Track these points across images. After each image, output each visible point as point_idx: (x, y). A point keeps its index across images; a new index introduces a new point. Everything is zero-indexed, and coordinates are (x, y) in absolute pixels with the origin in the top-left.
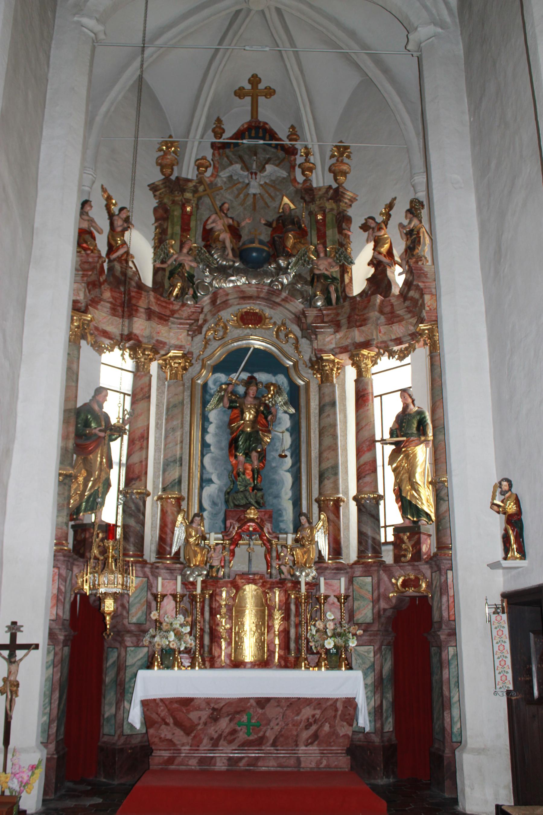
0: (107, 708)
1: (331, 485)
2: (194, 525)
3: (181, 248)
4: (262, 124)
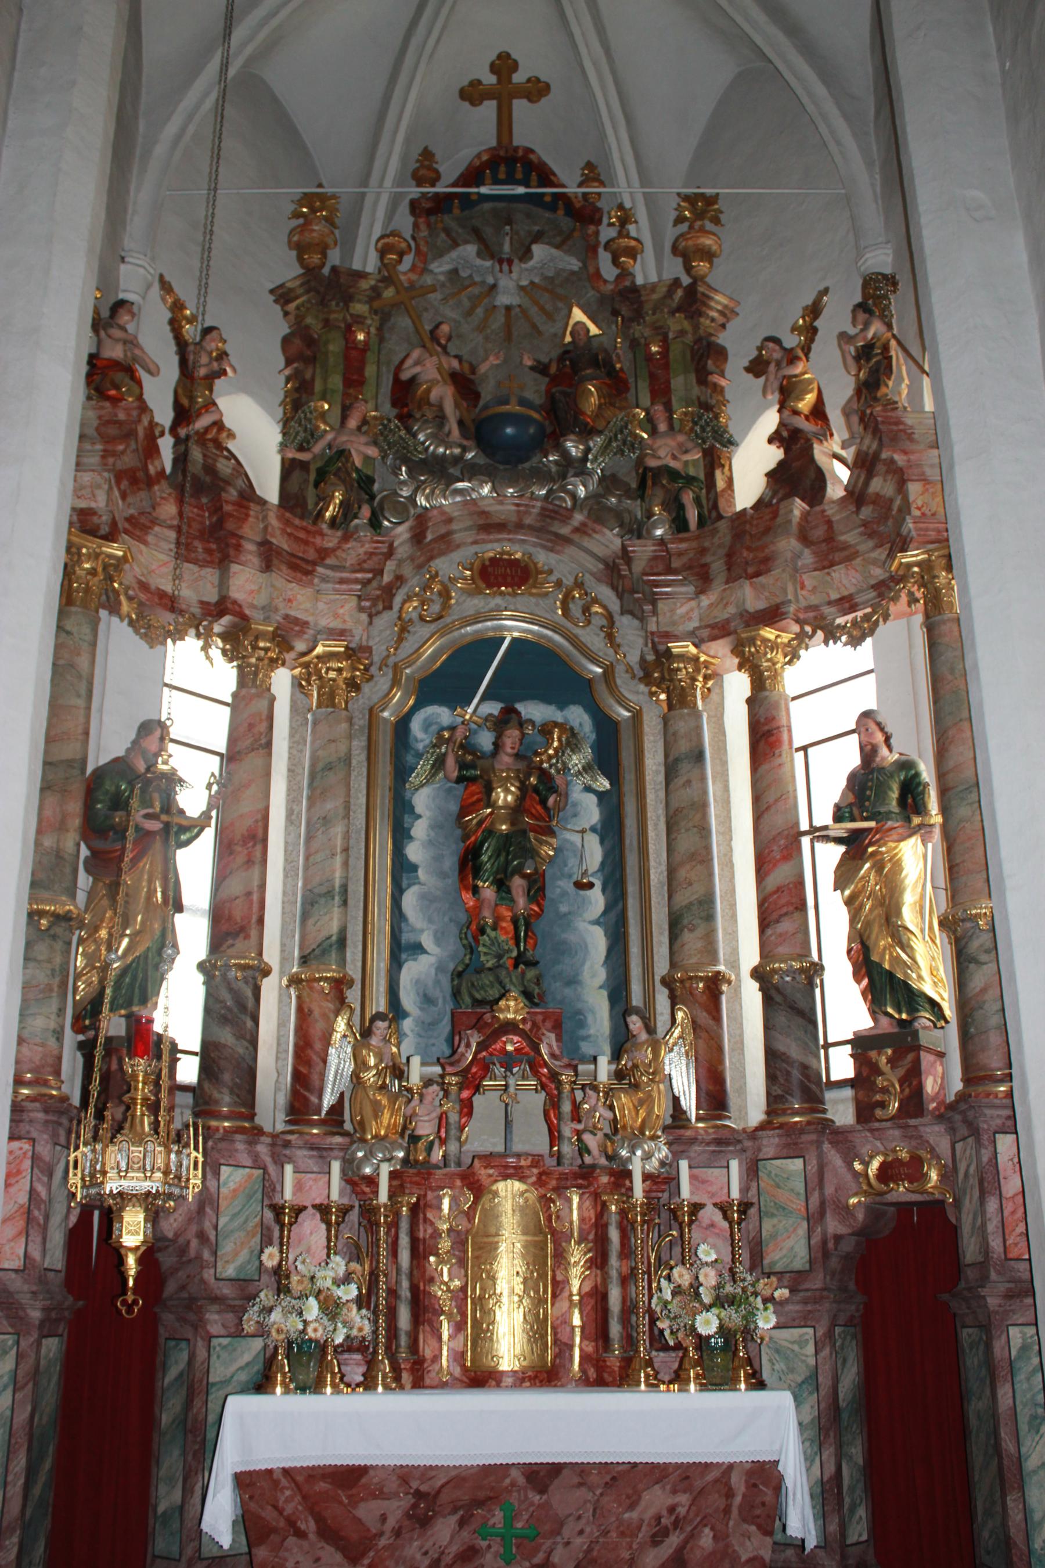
0: (162, 1489)
1: (699, 944)
2: (374, 1041)
3: (344, 418)
4: (520, 153)
